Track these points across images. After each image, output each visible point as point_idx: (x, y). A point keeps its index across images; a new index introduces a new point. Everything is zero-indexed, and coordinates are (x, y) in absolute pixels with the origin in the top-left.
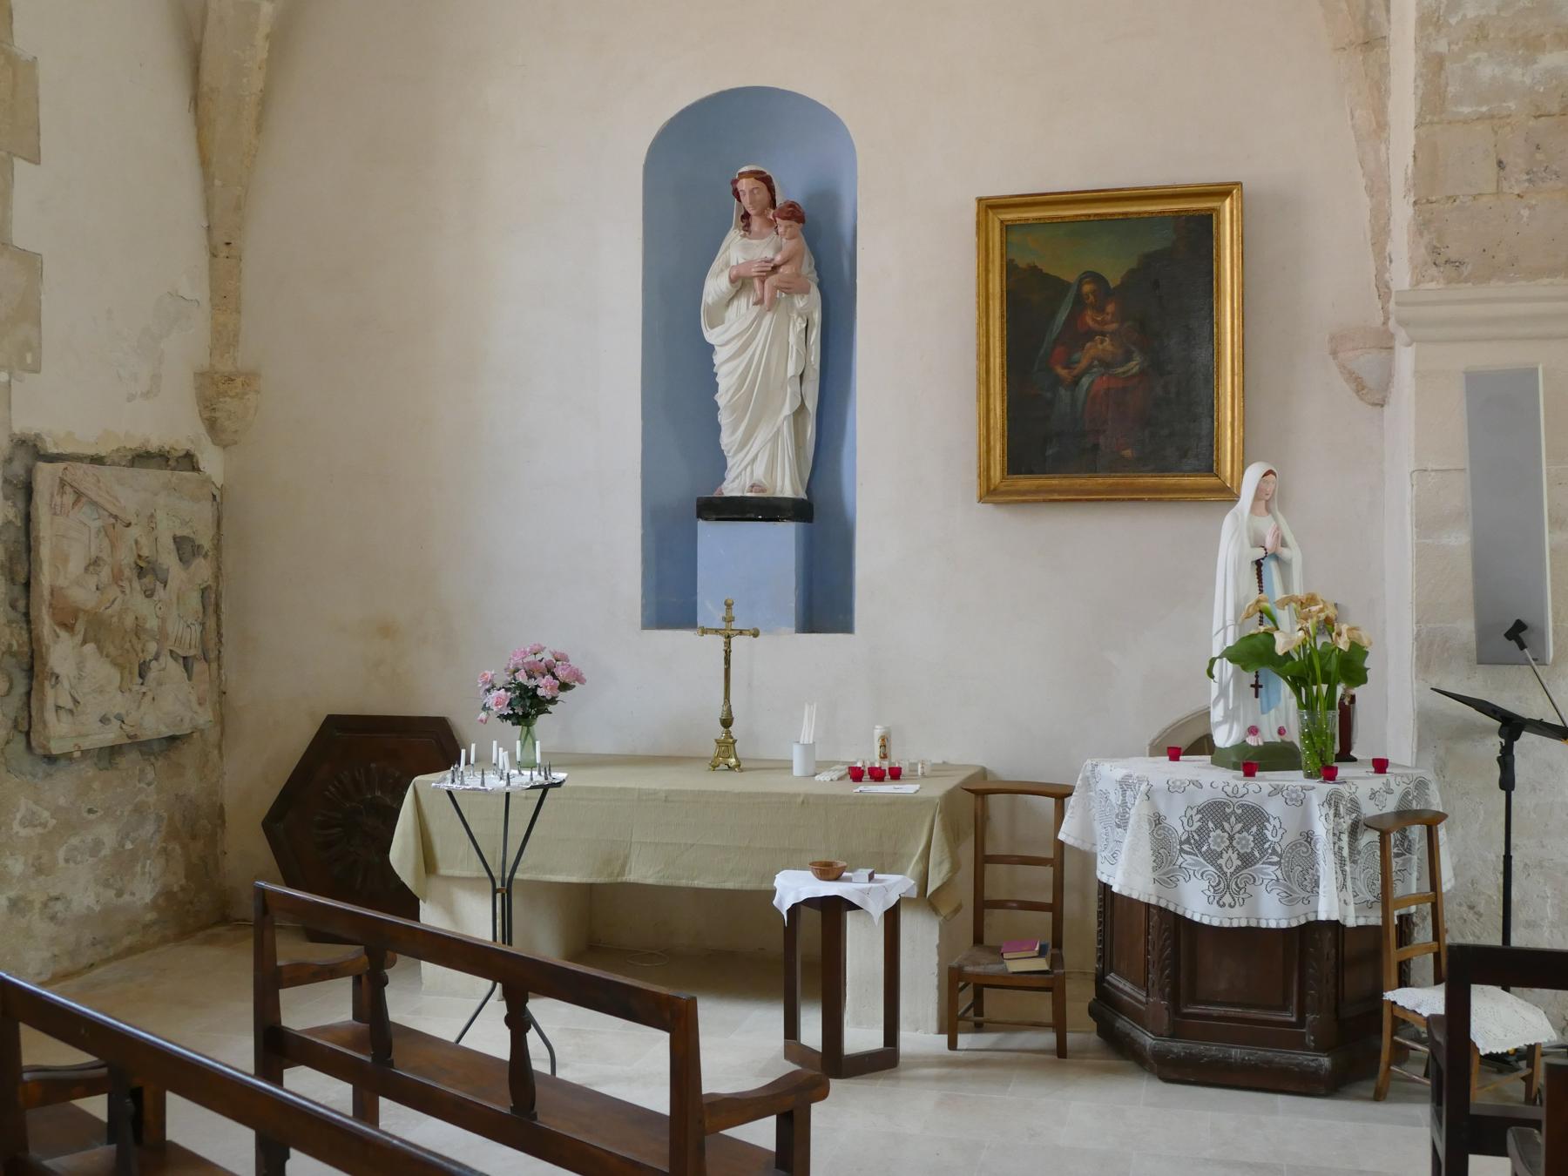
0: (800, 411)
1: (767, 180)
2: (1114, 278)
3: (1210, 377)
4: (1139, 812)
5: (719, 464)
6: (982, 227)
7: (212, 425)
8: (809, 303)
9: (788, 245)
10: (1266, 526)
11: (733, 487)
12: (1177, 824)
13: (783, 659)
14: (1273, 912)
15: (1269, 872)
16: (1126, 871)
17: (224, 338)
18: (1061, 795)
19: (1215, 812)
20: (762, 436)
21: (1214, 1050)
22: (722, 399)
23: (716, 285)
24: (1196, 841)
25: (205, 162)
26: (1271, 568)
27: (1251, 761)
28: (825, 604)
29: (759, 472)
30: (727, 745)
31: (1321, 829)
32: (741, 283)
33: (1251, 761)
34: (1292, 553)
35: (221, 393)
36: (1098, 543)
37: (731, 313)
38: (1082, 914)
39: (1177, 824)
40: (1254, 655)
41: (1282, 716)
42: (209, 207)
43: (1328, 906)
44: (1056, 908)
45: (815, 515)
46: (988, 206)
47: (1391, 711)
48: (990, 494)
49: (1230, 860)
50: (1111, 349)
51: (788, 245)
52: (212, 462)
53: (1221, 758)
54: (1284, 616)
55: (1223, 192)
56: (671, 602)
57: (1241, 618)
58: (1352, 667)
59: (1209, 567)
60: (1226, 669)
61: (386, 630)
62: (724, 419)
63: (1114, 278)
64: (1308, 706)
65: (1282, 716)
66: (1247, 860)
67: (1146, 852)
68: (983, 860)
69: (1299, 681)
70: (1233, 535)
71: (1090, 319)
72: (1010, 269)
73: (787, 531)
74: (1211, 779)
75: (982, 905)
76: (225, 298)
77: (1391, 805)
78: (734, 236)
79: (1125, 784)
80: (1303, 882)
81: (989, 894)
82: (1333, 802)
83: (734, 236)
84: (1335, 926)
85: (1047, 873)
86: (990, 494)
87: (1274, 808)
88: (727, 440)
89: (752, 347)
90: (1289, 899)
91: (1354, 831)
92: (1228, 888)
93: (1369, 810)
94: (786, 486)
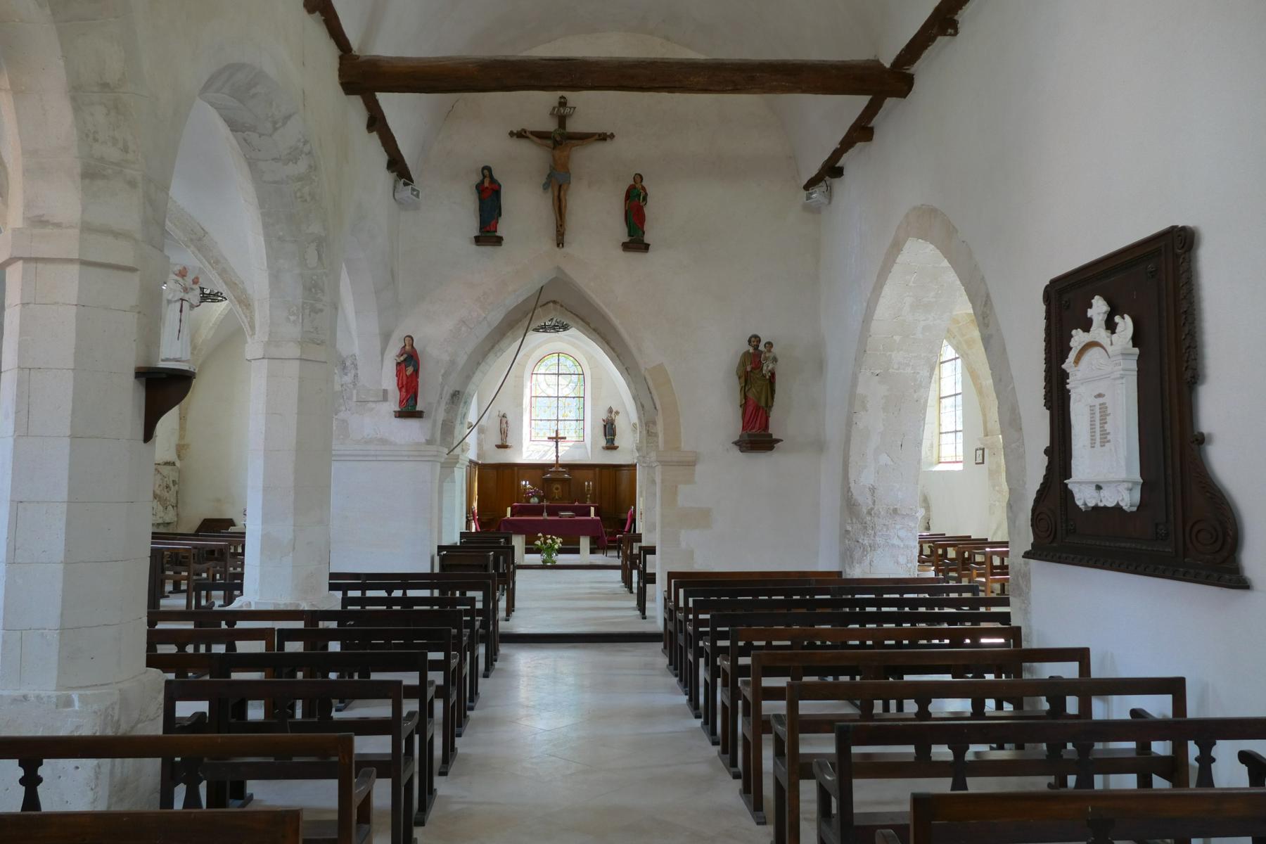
7: (179, 456)
17: (182, 437)
52: (178, 464)
61: (219, 500)
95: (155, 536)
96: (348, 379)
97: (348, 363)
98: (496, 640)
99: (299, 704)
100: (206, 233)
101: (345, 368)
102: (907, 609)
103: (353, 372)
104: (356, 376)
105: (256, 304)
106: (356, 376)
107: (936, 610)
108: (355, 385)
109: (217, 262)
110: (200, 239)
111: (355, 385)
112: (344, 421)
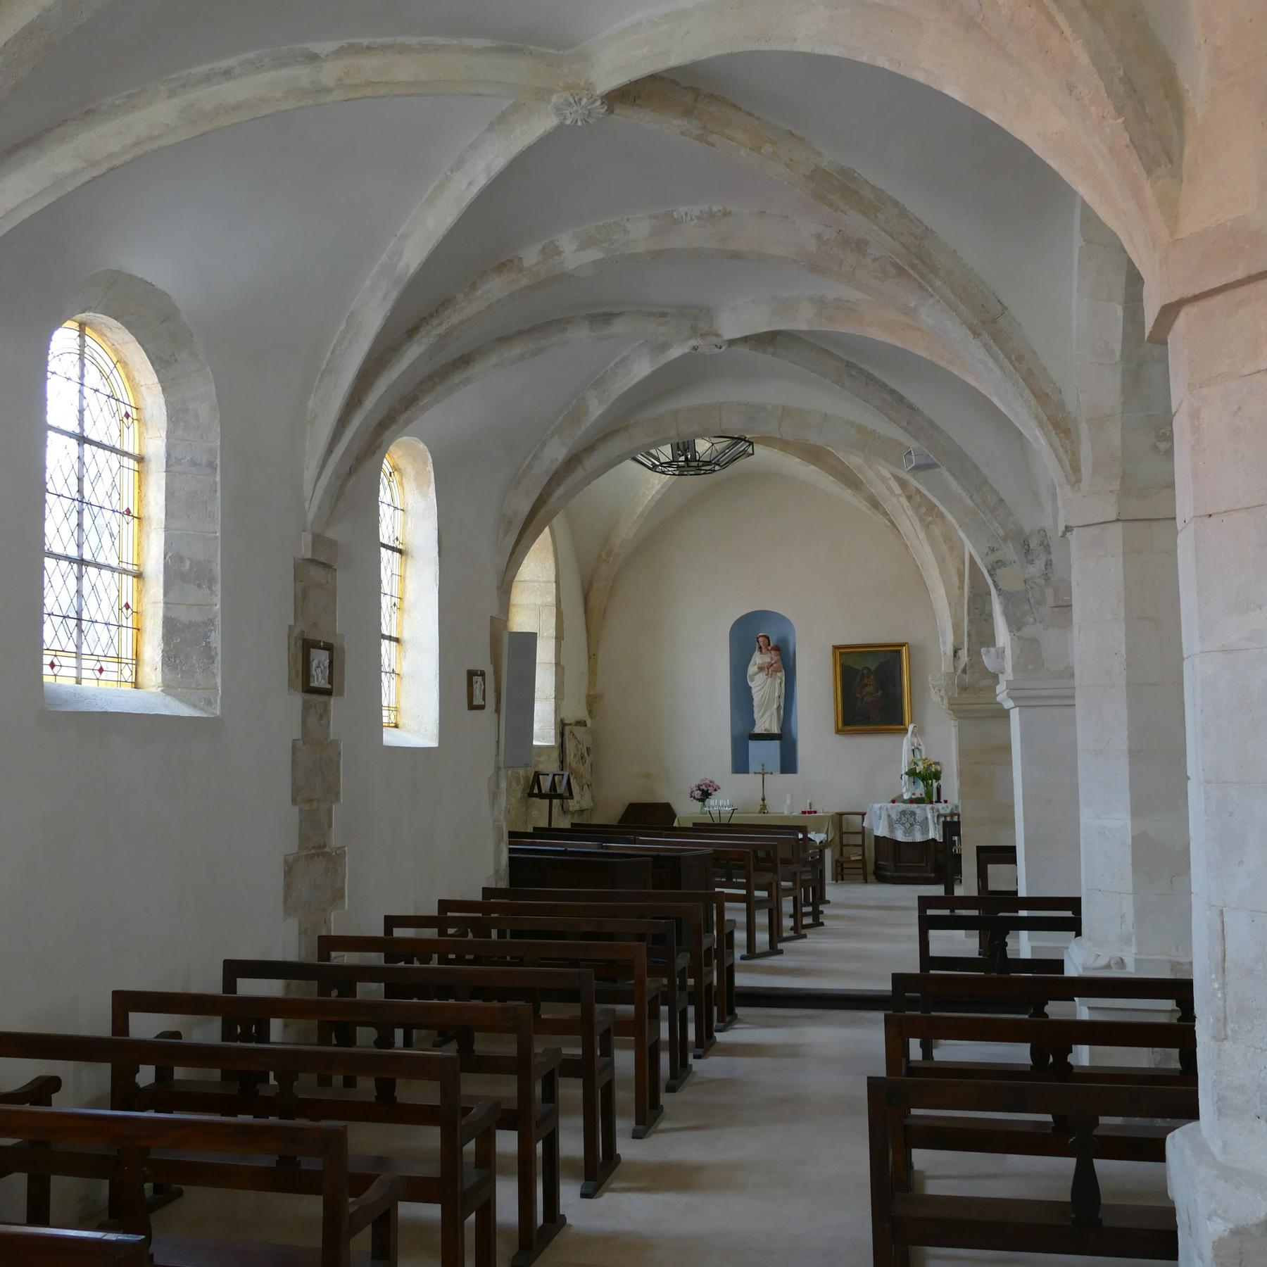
0: (779, 707)
1: (767, 638)
2: (873, 668)
3: (901, 696)
4: (884, 815)
5: (753, 723)
6: (834, 654)
7: (590, 712)
8: (781, 675)
9: (775, 658)
10: (915, 740)
11: (757, 730)
12: (894, 817)
13: (779, 781)
14: (919, 838)
15: (917, 827)
16: (881, 830)
17: (592, 684)
18: (863, 815)
19: (903, 813)
20: (768, 714)
21: (905, 874)
22: (755, 704)
23: (752, 669)
24: (899, 820)
25: (588, 630)
26: (917, 752)
27: (911, 801)
28: (788, 764)
29: (767, 726)
30: (764, 806)
31: (929, 816)
32: (761, 669)
33: (911, 801)
34: (922, 747)
35: (593, 701)
36: (870, 745)
37: (757, 677)
38: (870, 844)
39: (894, 817)
40: (912, 773)
41: (920, 790)
42: (588, 644)
43: (931, 835)
44: (863, 846)
45: (785, 738)
46: (836, 648)
47: (951, 786)
48: (838, 731)
49: (908, 825)
50: (873, 691)
51: (775, 658)
52: (589, 723)
53: (905, 802)
54: (920, 763)
55: (902, 645)
56: (741, 765)
57: (909, 764)
58: (937, 776)
59: (901, 750)
60: (906, 777)
61: (647, 776)
62: (756, 709)
63: (873, 668)
64: (926, 786)
65: (920, 790)
66: (912, 825)
67: (886, 825)
68: (842, 833)
69: (923, 780)
70: (906, 742)
71: (866, 680)
72: (843, 666)
73: (777, 743)
74: (903, 806)
75: (842, 846)
76: (592, 672)
77: (948, 811)
78: (757, 654)
79: (881, 808)
80: (925, 829)
81: (845, 842)
82: (932, 809)
83: (757, 654)
84: (934, 840)
85: (859, 850)
86: (838, 731)
87: (918, 811)
88: (756, 716)
89: (764, 687)
90: (923, 834)
91: (938, 817)
92: (909, 831)
93: (942, 812)
94: (775, 730)
95: (513, 835)
96: (1036, 569)
97: (1034, 543)
98: (731, 1001)
99: (272, 1074)
100: (1005, 308)
101: (1028, 551)
102: (417, 964)
103: (1043, 558)
104: (1049, 564)
105: (1084, 429)
106: (1049, 564)
107: (417, 964)
108: (1047, 579)
109: (1020, 359)
110: (994, 321)
111: (1047, 579)
112: (1034, 641)
